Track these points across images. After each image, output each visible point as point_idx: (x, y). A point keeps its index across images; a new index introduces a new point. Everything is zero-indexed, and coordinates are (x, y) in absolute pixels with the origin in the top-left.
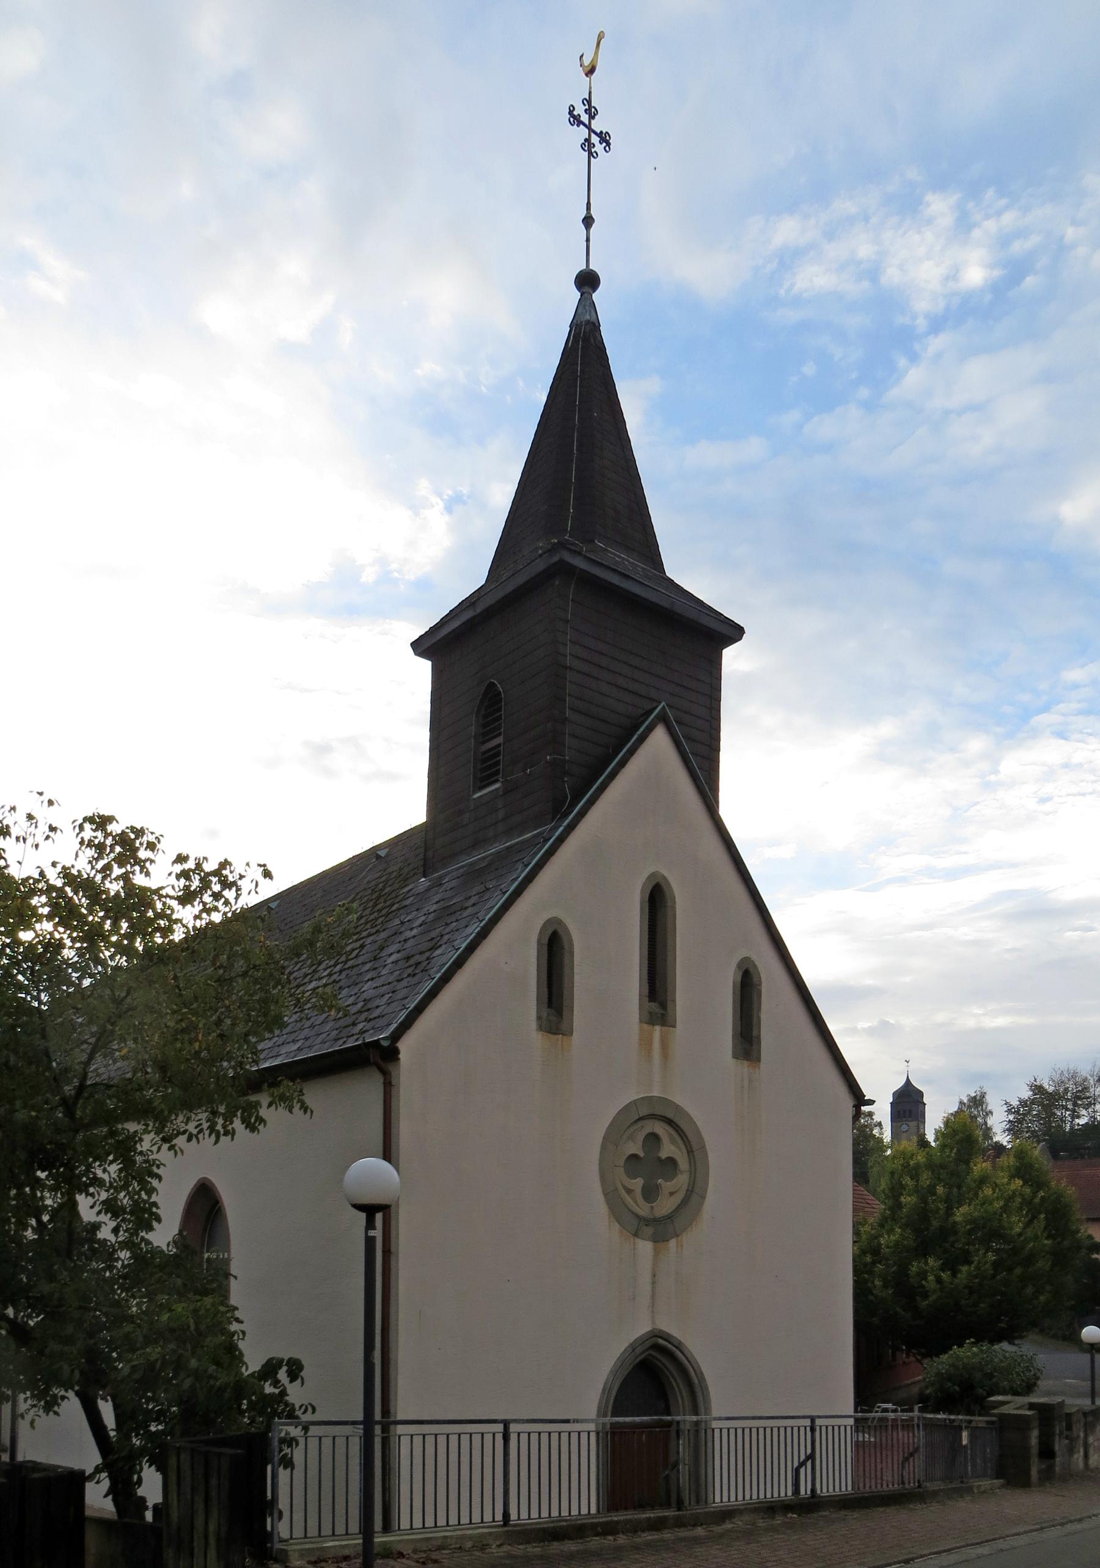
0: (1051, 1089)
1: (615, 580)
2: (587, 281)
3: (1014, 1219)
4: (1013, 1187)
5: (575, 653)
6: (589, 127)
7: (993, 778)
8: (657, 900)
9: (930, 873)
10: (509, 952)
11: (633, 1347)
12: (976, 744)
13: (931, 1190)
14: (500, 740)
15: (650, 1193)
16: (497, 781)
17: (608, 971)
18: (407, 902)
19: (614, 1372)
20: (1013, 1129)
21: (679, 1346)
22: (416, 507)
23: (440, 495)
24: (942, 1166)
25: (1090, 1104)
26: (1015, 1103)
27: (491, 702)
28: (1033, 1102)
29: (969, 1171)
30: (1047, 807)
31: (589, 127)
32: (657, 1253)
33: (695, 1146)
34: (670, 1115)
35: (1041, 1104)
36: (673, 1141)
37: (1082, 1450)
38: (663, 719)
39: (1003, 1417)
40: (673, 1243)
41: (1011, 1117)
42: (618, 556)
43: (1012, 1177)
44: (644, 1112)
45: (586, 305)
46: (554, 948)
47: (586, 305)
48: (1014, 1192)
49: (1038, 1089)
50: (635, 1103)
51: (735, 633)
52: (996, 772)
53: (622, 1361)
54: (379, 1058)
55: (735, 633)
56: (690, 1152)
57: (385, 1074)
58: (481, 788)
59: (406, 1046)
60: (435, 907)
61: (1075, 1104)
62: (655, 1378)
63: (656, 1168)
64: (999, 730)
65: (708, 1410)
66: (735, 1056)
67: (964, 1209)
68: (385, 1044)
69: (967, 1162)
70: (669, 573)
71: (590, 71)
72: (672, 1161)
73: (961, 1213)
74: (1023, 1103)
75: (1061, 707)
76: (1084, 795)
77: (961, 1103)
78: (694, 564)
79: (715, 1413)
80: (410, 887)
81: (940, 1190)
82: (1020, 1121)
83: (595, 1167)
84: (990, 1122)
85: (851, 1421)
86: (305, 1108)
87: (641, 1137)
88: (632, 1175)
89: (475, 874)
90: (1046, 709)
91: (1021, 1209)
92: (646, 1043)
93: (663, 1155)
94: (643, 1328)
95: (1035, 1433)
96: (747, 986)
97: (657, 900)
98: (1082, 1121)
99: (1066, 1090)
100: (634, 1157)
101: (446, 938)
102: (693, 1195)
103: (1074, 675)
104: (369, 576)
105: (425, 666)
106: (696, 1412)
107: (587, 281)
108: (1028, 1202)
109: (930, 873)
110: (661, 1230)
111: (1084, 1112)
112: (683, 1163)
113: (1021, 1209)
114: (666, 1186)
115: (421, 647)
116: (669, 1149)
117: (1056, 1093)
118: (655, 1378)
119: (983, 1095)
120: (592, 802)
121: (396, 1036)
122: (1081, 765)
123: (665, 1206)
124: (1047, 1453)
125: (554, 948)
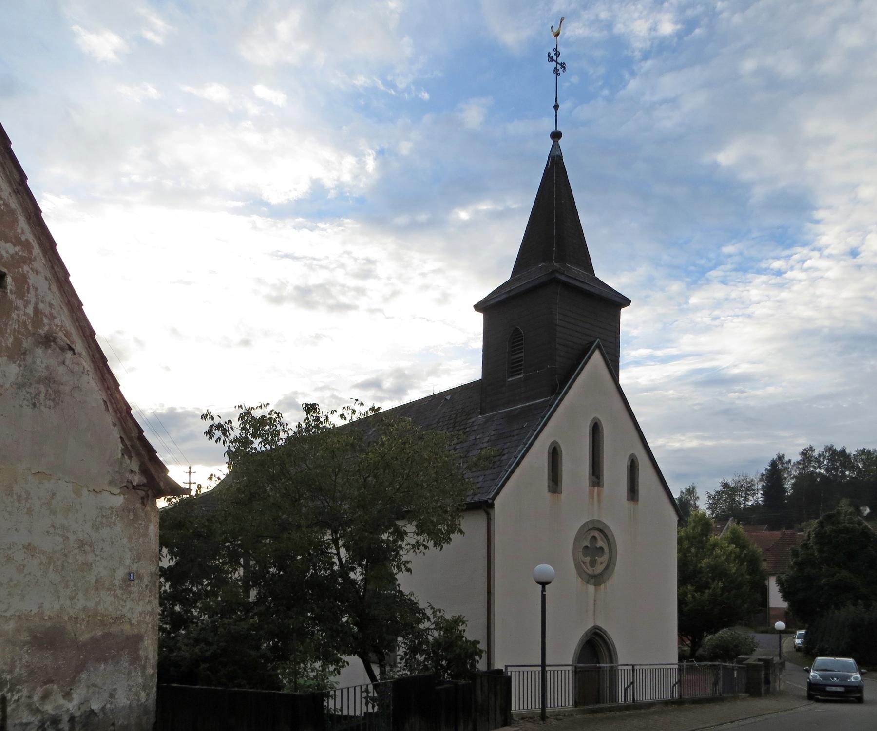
0: (733, 485)
1: (578, 284)
2: (556, 136)
3: (732, 565)
4: (730, 548)
5: (553, 313)
6: (557, 63)
7: (685, 306)
8: (596, 429)
9: (651, 358)
10: (537, 457)
11: (586, 633)
12: (675, 287)
13: (688, 550)
14: (522, 354)
15: (593, 563)
16: (520, 374)
17: (575, 465)
18: (475, 428)
19: (579, 645)
20: (712, 507)
21: (605, 633)
22: (360, 156)
23: (373, 149)
24: (694, 538)
25: (754, 494)
26: (713, 493)
27: (516, 338)
28: (723, 492)
29: (707, 540)
30: (716, 323)
31: (557, 63)
32: (596, 590)
33: (611, 541)
34: (601, 527)
35: (727, 493)
36: (602, 540)
37: (607, 653)
38: (598, 347)
39: (749, 665)
40: (602, 586)
41: (711, 501)
42: (576, 270)
43: (730, 543)
44: (590, 527)
45: (556, 147)
46: (555, 454)
47: (556, 147)
48: (732, 551)
49: (726, 485)
50: (587, 523)
51: (627, 302)
52: (687, 303)
53: (581, 640)
54: (486, 507)
55: (627, 302)
56: (609, 544)
57: (488, 514)
58: (512, 376)
59: (497, 502)
60: (493, 433)
61: (746, 494)
62: (595, 645)
63: (595, 550)
64: (688, 280)
65: (617, 661)
66: (628, 500)
67: (706, 560)
68: (490, 501)
69: (706, 536)
70: (598, 274)
71: (557, 35)
72: (601, 549)
73: (705, 562)
74: (718, 493)
75: (722, 267)
76: (738, 316)
77: (682, 492)
78: (609, 273)
79: (620, 662)
80: (473, 420)
81: (693, 550)
82: (715, 503)
83: (571, 554)
84: (698, 503)
85: (676, 666)
86: (461, 532)
87: (589, 537)
88: (585, 556)
89: (511, 418)
90: (713, 268)
91: (735, 560)
92: (591, 494)
93: (598, 546)
94: (590, 625)
95: (763, 672)
96: (633, 467)
97: (596, 429)
98: (750, 503)
99: (742, 486)
100: (586, 547)
101: (506, 451)
102: (610, 564)
103: (729, 249)
104: (332, 194)
105: (480, 317)
106: (611, 662)
107: (556, 136)
108: (738, 557)
109: (651, 358)
110: (597, 580)
111: (751, 498)
112: (606, 549)
113: (735, 560)
114: (600, 560)
115: (478, 307)
116: (600, 543)
117: (736, 487)
118: (595, 645)
119: (694, 488)
120: (570, 387)
121: (494, 498)
122: (735, 299)
123: (599, 569)
124: (767, 682)
125: (555, 454)
